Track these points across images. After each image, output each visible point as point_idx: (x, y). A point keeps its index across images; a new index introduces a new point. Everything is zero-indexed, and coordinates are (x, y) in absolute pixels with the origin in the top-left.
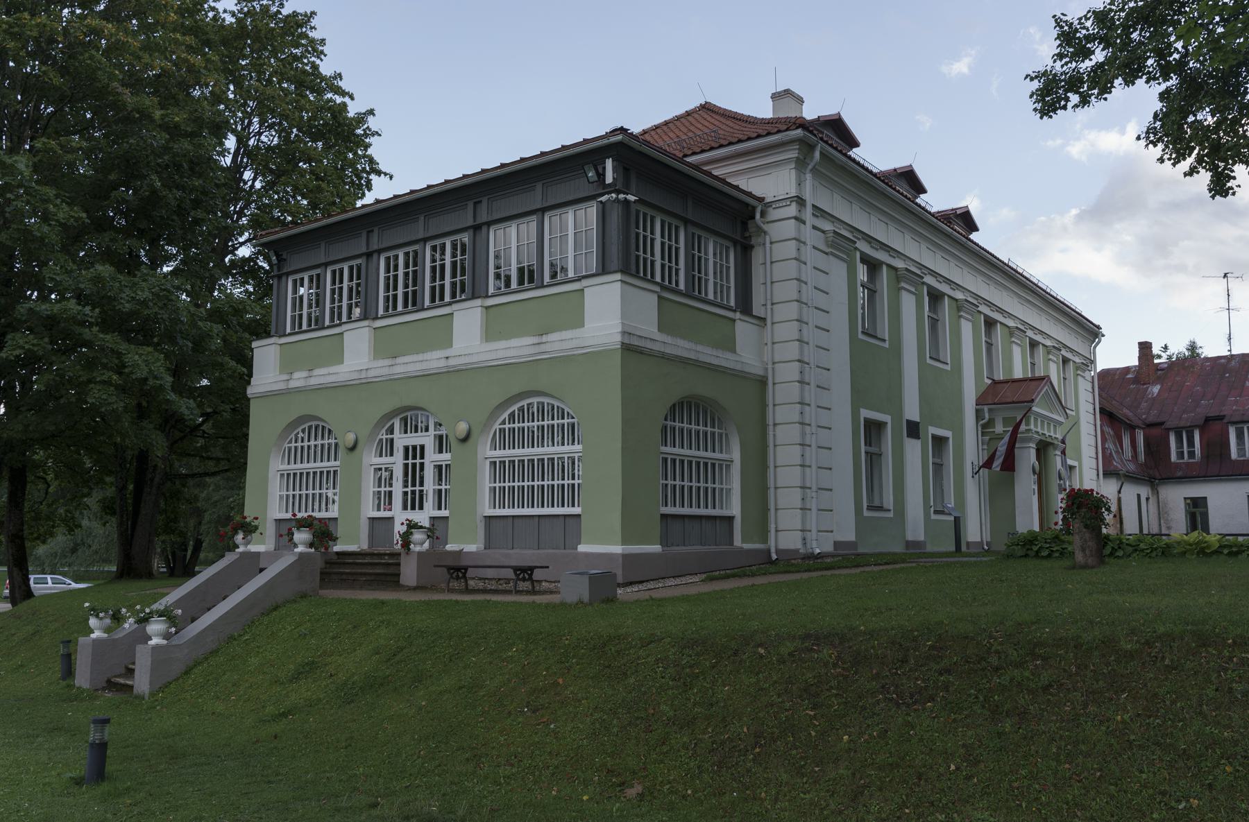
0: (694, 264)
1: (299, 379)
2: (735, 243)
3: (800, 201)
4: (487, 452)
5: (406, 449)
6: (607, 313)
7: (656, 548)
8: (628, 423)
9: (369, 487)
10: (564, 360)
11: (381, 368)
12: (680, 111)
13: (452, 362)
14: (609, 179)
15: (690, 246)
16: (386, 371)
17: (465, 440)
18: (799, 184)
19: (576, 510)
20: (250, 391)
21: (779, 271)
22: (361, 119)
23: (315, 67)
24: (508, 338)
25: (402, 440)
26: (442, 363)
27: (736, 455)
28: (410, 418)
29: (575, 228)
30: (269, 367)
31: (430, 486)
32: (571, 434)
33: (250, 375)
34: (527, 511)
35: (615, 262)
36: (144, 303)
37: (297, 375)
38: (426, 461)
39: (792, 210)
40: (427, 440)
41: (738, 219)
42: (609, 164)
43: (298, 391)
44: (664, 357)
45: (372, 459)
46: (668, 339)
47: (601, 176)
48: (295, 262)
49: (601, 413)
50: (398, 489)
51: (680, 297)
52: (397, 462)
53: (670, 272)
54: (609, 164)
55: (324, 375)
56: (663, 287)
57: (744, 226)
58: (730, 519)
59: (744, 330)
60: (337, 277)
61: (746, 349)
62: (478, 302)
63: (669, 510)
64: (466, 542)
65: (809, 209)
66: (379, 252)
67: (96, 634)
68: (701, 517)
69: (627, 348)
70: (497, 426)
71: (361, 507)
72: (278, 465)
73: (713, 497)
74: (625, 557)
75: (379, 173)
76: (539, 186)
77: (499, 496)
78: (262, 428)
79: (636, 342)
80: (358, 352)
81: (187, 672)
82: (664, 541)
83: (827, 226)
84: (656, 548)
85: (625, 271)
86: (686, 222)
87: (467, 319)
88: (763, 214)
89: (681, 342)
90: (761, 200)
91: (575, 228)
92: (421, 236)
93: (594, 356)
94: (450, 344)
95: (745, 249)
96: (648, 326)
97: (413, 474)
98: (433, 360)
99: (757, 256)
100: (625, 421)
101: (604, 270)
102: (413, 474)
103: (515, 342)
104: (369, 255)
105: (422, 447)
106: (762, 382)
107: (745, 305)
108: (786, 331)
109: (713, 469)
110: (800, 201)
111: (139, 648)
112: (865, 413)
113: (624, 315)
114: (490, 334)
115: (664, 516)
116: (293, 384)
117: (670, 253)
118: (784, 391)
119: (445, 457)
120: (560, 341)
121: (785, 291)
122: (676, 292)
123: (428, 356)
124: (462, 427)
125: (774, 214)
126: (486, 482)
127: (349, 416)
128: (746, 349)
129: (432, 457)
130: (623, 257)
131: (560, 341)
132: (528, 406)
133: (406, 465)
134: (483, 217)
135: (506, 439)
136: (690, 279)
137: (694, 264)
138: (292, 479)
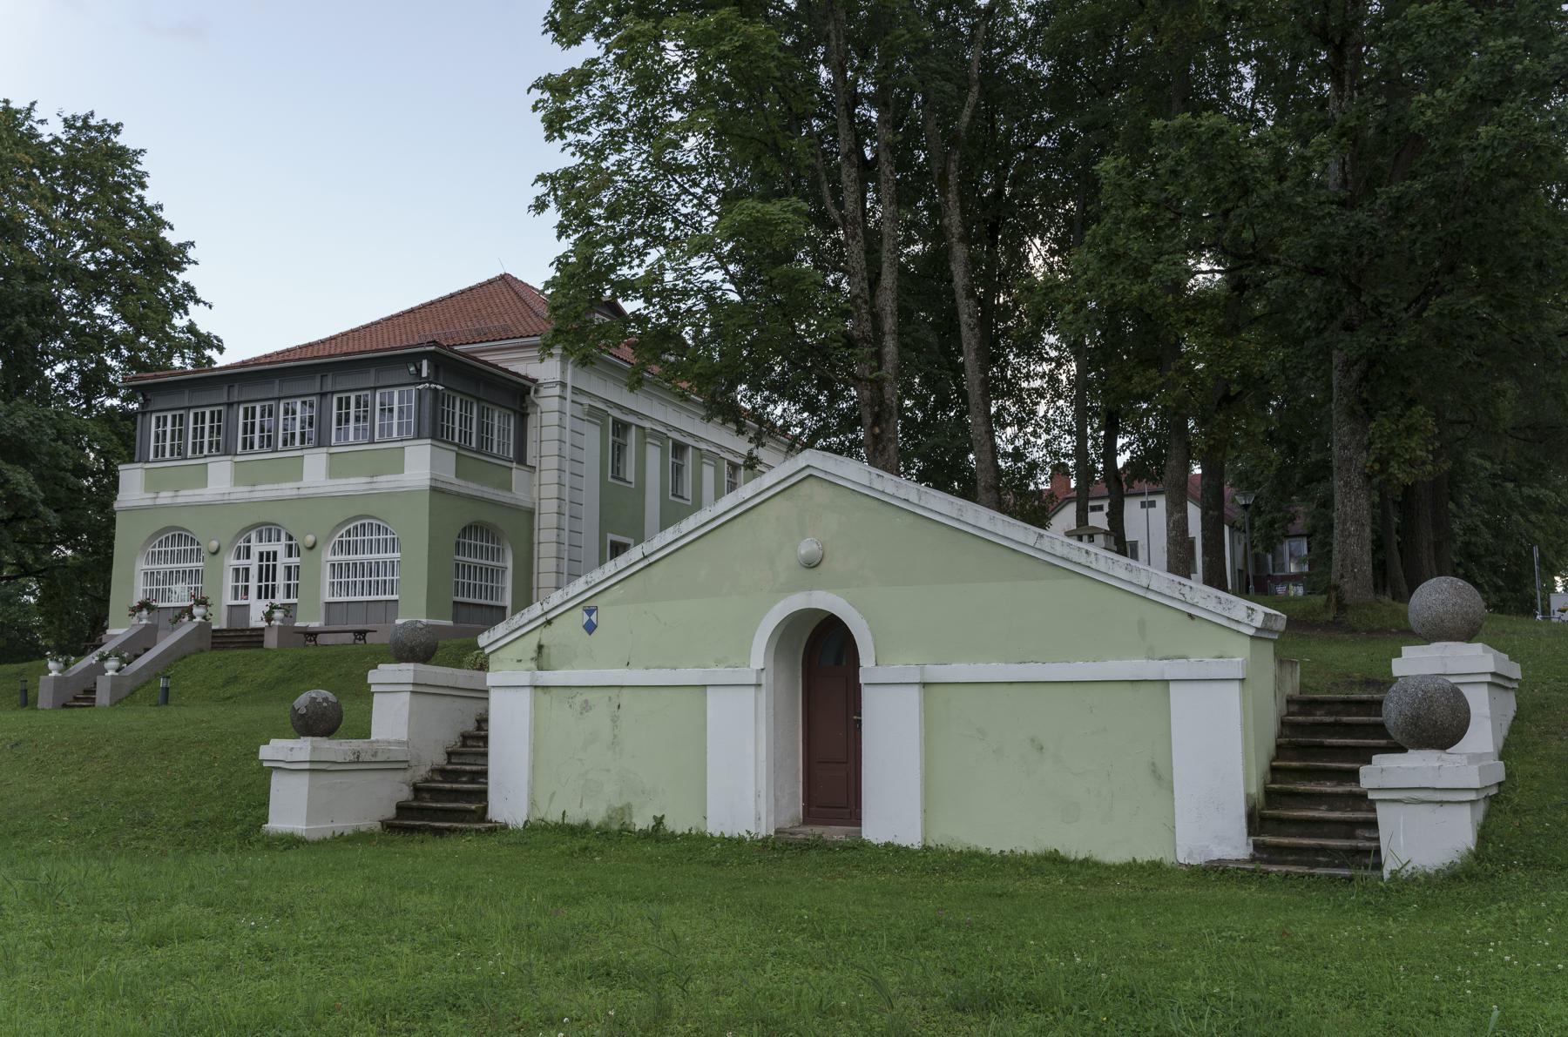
0: (484, 429)
1: (165, 497)
2: (515, 412)
3: (563, 385)
4: (328, 557)
5: (261, 554)
6: (420, 464)
7: (450, 623)
8: (432, 539)
9: (229, 582)
10: (389, 495)
11: (242, 493)
12: (483, 279)
13: (302, 492)
14: (424, 374)
15: (481, 416)
16: (247, 495)
17: (312, 548)
18: (563, 372)
19: (395, 597)
20: (116, 505)
21: (546, 434)
22: (183, 247)
23: (141, 199)
24: (347, 477)
25: (257, 548)
26: (295, 492)
27: (509, 564)
28: (267, 529)
29: (401, 399)
30: (133, 487)
31: (281, 580)
32: (394, 545)
33: (116, 488)
34: (358, 598)
35: (426, 430)
36: (21, 431)
37: (162, 494)
38: (278, 563)
39: (557, 390)
40: (280, 547)
41: (517, 396)
42: (425, 363)
43: (164, 506)
44: (459, 495)
45: (231, 561)
46: (462, 483)
47: (419, 371)
48: (158, 403)
49: (415, 531)
50: (253, 584)
51: (473, 453)
52: (254, 563)
53: (466, 435)
54: (425, 363)
55: (188, 496)
56: (458, 445)
57: (523, 400)
58: (504, 608)
59: (517, 474)
60: (200, 418)
61: (520, 489)
62: (324, 450)
63: (459, 599)
64: (311, 620)
65: (569, 389)
66: (239, 403)
67: (54, 674)
68: (481, 606)
69: (433, 489)
70: (336, 539)
71: (230, 596)
72: (142, 565)
73: (495, 592)
74: (427, 626)
75: (197, 301)
76: (373, 371)
77: (336, 587)
78: (126, 539)
79: (439, 485)
80: (221, 478)
81: (133, 693)
82: (455, 619)
83: (585, 401)
84: (450, 623)
85: (433, 437)
86: (479, 400)
87: (315, 463)
88: (536, 391)
89: (470, 485)
90: (534, 381)
91: (401, 399)
92: (276, 395)
93: (411, 494)
94: (301, 479)
95: (522, 417)
96: (449, 475)
97: (267, 573)
98: (287, 489)
99: (532, 421)
100: (431, 538)
101: (419, 436)
102: (267, 573)
103: (352, 480)
104: (230, 405)
105: (275, 553)
106: (530, 513)
107: (521, 458)
108: (549, 477)
109: (495, 573)
110: (563, 385)
111: (99, 678)
112: (611, 537)
113: (432, 467)
114: (332, 473)
115: (455, 603)
116: (159, 502)
117: (465, 421)
118: (547, 520)
119: (295, 560)
120: (386, 482)
121: (550, 448)
122: (471, 450)
123: (283, 485)
124: (310, 539)
125: (544, 392)
126: (327, 578)
127: (193, 527)
128: (520, 489)
129: (283, 560)
130: (435, 429)
131: (386, 482)
132: (360, 523)
133: (261, 567)
134: (328, 387)
135: (343, 547)
136: (480, 440)
137: (484, 429)
138: (149, 576)
